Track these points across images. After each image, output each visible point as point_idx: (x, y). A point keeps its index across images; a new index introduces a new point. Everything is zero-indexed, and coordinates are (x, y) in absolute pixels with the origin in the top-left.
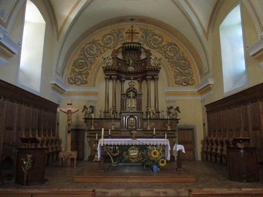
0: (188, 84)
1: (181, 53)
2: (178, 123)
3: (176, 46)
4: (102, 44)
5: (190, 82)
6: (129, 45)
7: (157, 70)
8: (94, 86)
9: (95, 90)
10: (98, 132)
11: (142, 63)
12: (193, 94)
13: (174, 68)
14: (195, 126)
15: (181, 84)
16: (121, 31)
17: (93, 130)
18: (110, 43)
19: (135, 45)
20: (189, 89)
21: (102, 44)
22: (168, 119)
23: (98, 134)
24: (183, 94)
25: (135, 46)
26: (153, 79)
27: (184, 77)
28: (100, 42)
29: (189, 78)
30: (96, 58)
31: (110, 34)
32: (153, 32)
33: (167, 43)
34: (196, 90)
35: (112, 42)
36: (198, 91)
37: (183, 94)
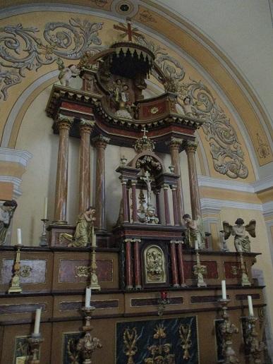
0: (238, 176)
1: (219, 109)
2: (254, 262)
3: (208, 92)
4: (45, 43)
5: (241, 172)
6: (125, 50)
7: (190, 126)
8: (13, 145)
9: (17, 159)
10: (253, 291)
11: (151, 107)
12: (248, 198)
13: (210, 135)
14: (262, 272)
15: (226, 173)
16: (94, 27)
17: (202, 289)
18: (67, 46)
19: (139, 52)
20: (240, 186)
21: (45, 43)
22: (237, 254)
23: (255, 297)
24: (230, 195)
25: (132, 52)
26: (184, 147)
27: (228, 159)
28: (40, 36)
29: (238, 163)
30: (25, 71)
31: (65, 26)
32: (165, 52)
33: (190, 82)
34: (253, 190)
35: (73, 46)
36: (258, 193)
37: (230, 195)
